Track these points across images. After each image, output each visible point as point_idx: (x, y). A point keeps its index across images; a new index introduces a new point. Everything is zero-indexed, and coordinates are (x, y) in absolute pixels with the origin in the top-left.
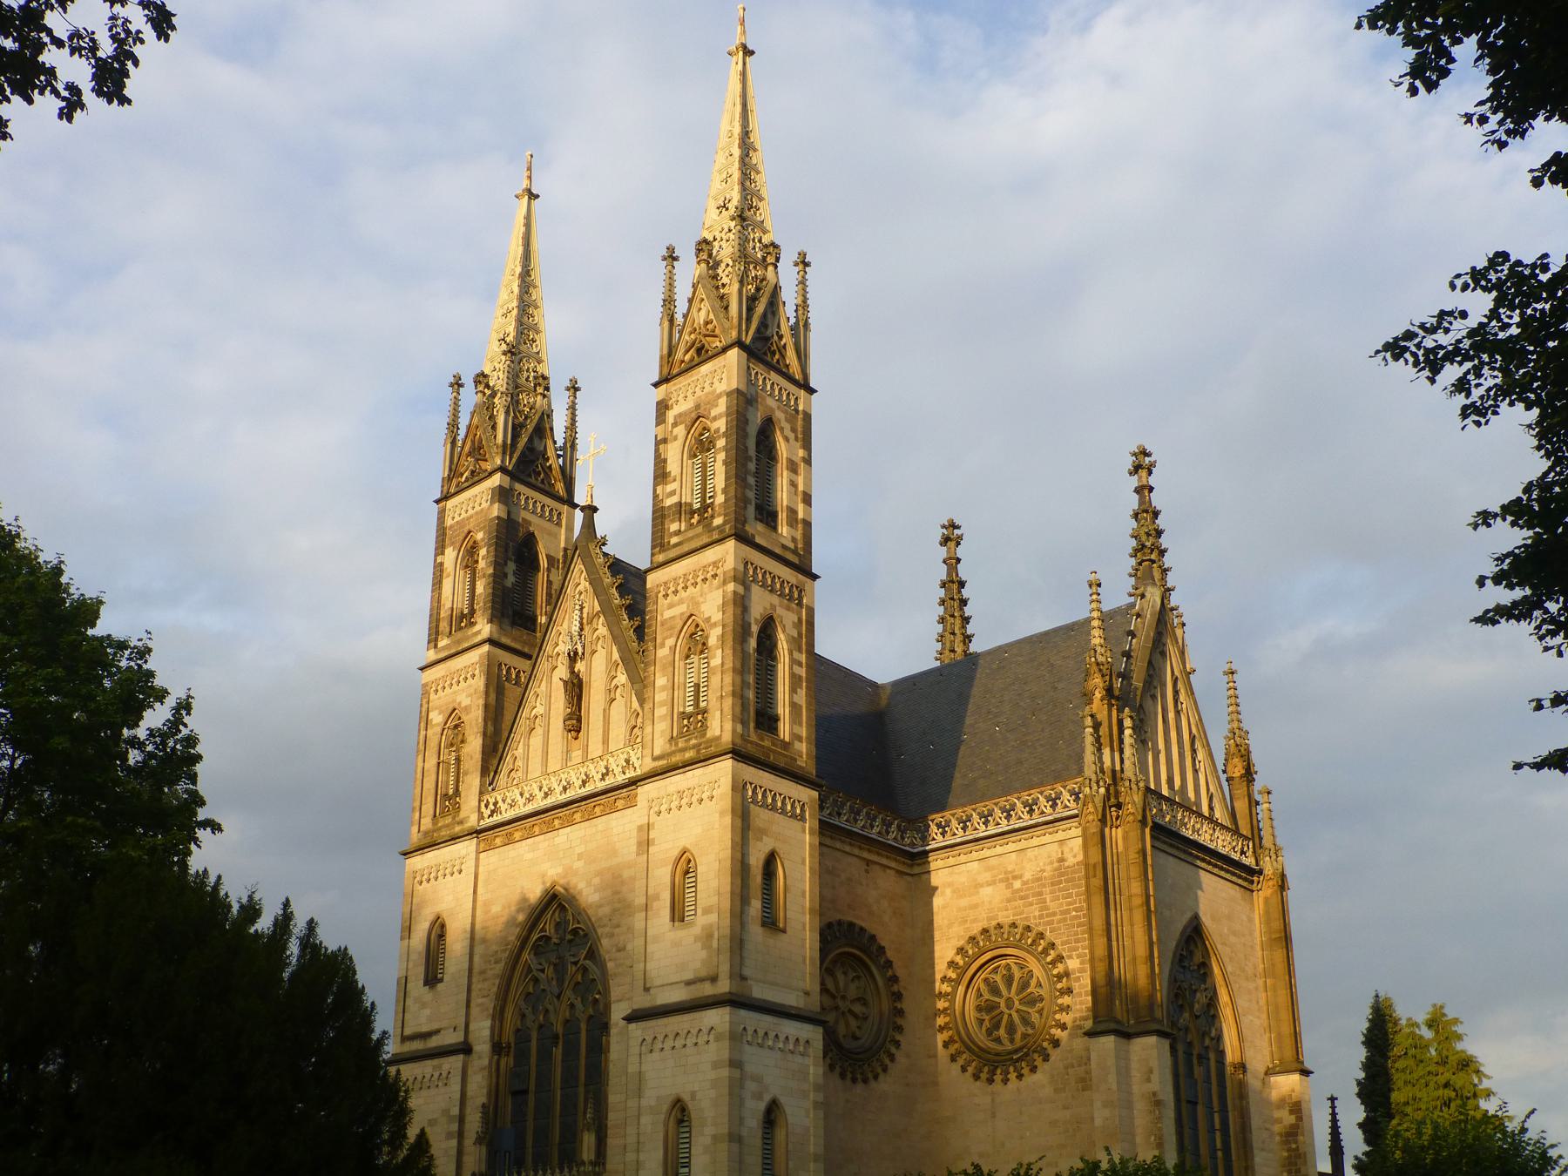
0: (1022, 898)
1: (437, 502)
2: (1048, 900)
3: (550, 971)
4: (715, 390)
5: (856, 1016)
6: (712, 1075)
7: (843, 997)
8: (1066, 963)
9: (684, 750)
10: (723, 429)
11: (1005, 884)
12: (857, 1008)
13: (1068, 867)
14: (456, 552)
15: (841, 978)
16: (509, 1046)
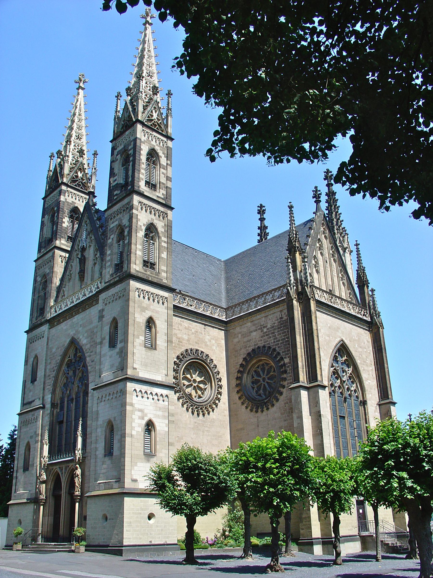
0: (267, 335)
9: (115, 278)
16: (57, 404)
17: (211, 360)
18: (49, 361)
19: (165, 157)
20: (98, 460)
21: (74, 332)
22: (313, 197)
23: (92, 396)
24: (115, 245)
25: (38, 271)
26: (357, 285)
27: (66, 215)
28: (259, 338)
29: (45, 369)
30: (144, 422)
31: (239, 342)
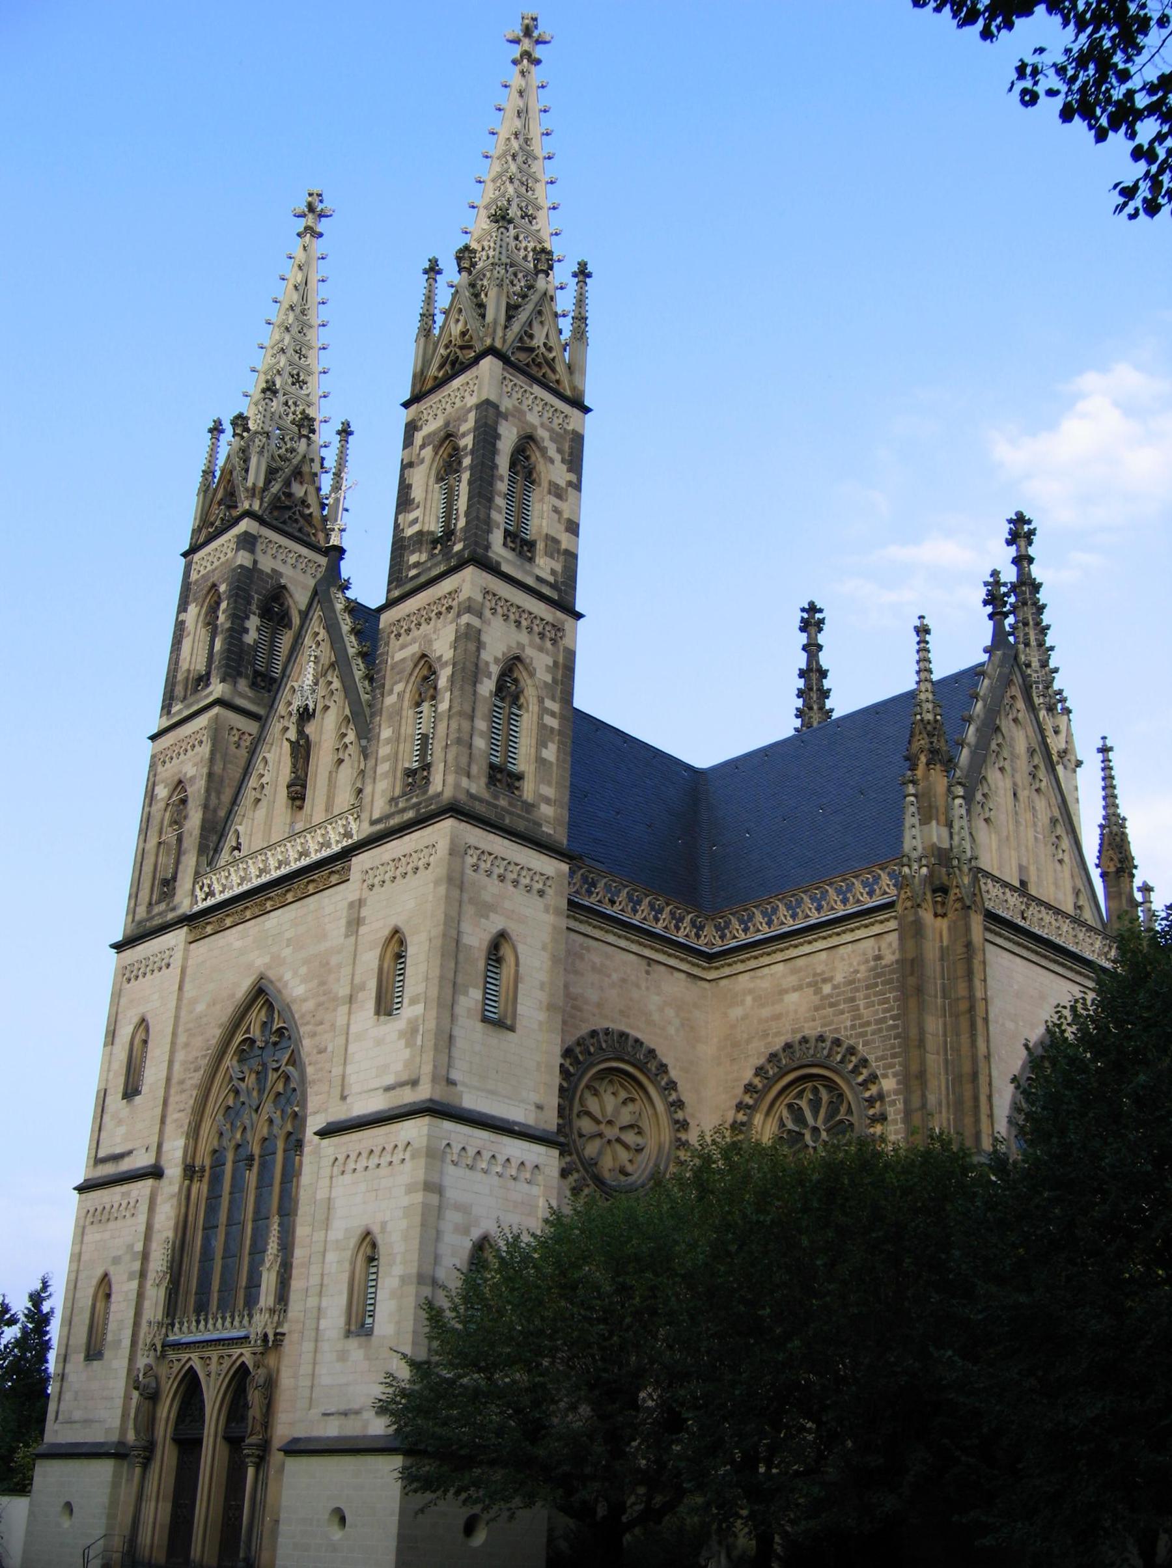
0: (832, 1005)
1: (185, 555)
2: (862, 1007)
3: (251, 1080)
4: (466, 404)
5: (627, 1147)
6: (405, 1201)
8: (880, 1083)
9: (404, 810)
10: (470, 446)
11: (813, 989)
12: (630, 1138)
13: (886, 966)
14: (199, 608)
16: (203, 1170)
18: (182, 1039)
19: (563, 461)
20: (325, 1346)
21: (267, 959)
22: (986, 603)
23: (317, 1151)
24: (408, 713)
25: (160, 769)
26: (1099, 870)
27: (254, 608)
29: (171, 1063)
31: (745, 1017)
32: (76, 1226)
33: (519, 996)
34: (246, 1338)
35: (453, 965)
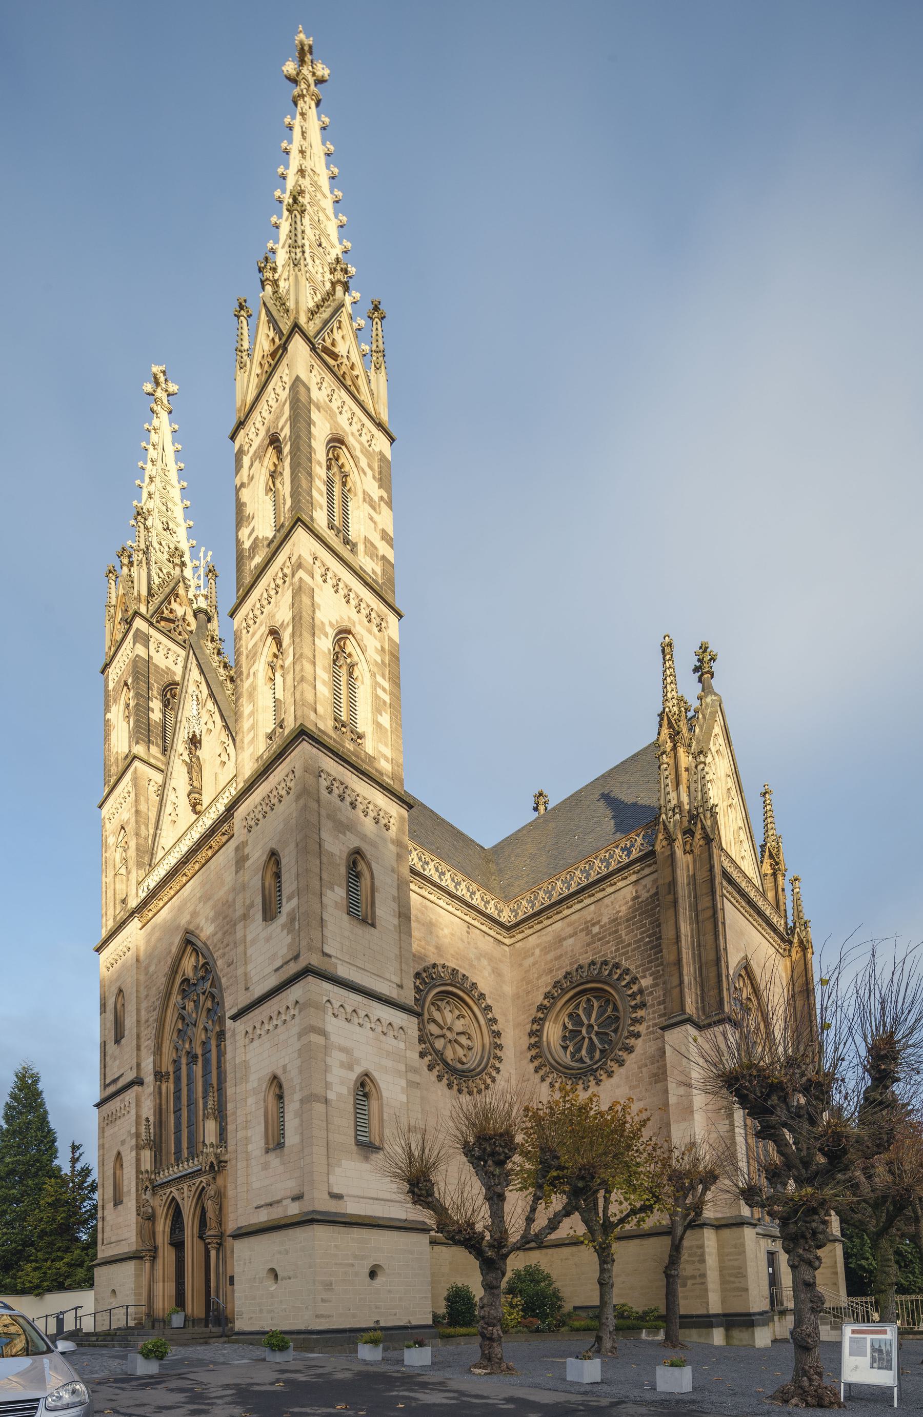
0: (600, 940)
2: (623, 935)
5: (462, 1046)
7: (449, 1029)
12: (463, 1040)
13: (642, 902)
15: (447, 1013)
16: (168, 1074)
17: (482, 994)
19: (374, 477)
27: (155, 693)
28: (583, 946)
30: (353, 1076)
31: (534, 964)
32: (99, 1128)
33: (377, 902)
34: (201, 1170)
35: (318, 862)
